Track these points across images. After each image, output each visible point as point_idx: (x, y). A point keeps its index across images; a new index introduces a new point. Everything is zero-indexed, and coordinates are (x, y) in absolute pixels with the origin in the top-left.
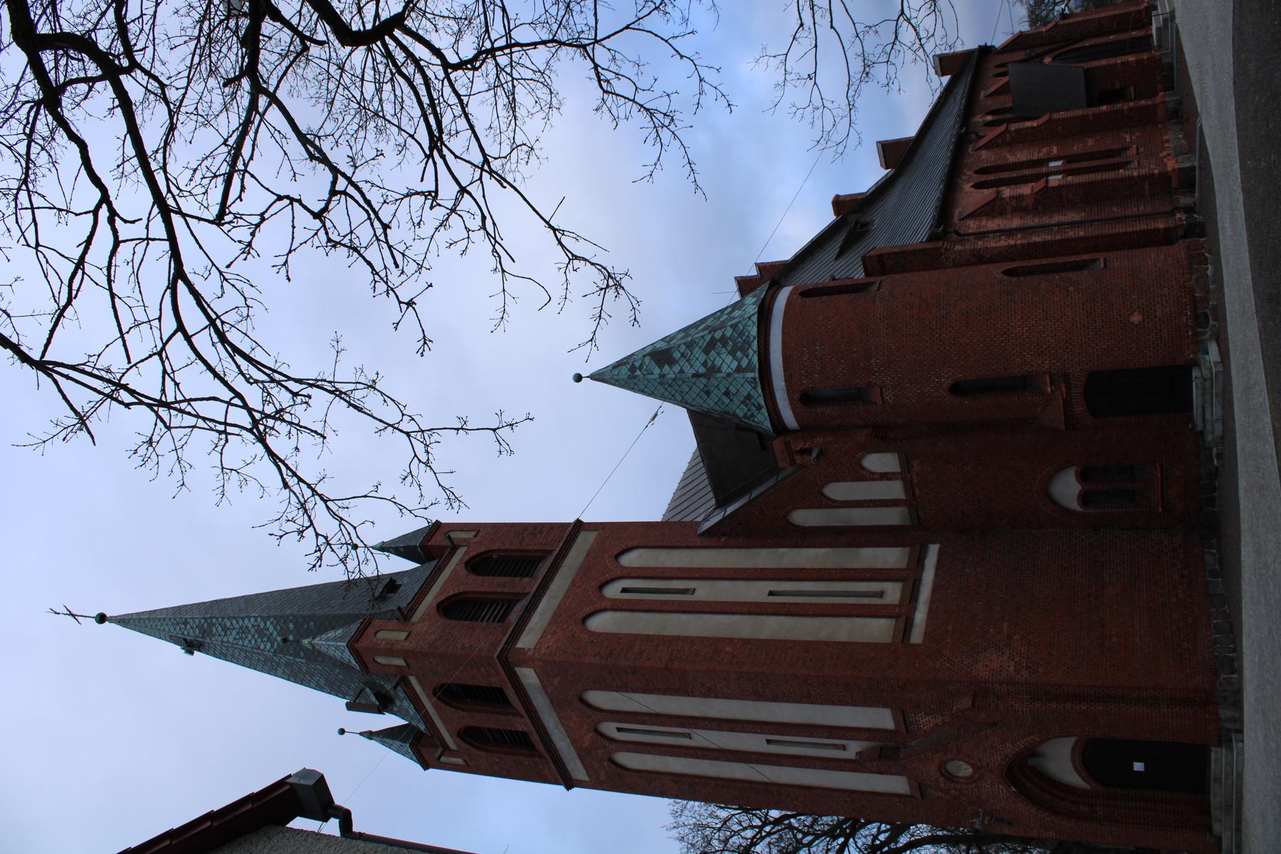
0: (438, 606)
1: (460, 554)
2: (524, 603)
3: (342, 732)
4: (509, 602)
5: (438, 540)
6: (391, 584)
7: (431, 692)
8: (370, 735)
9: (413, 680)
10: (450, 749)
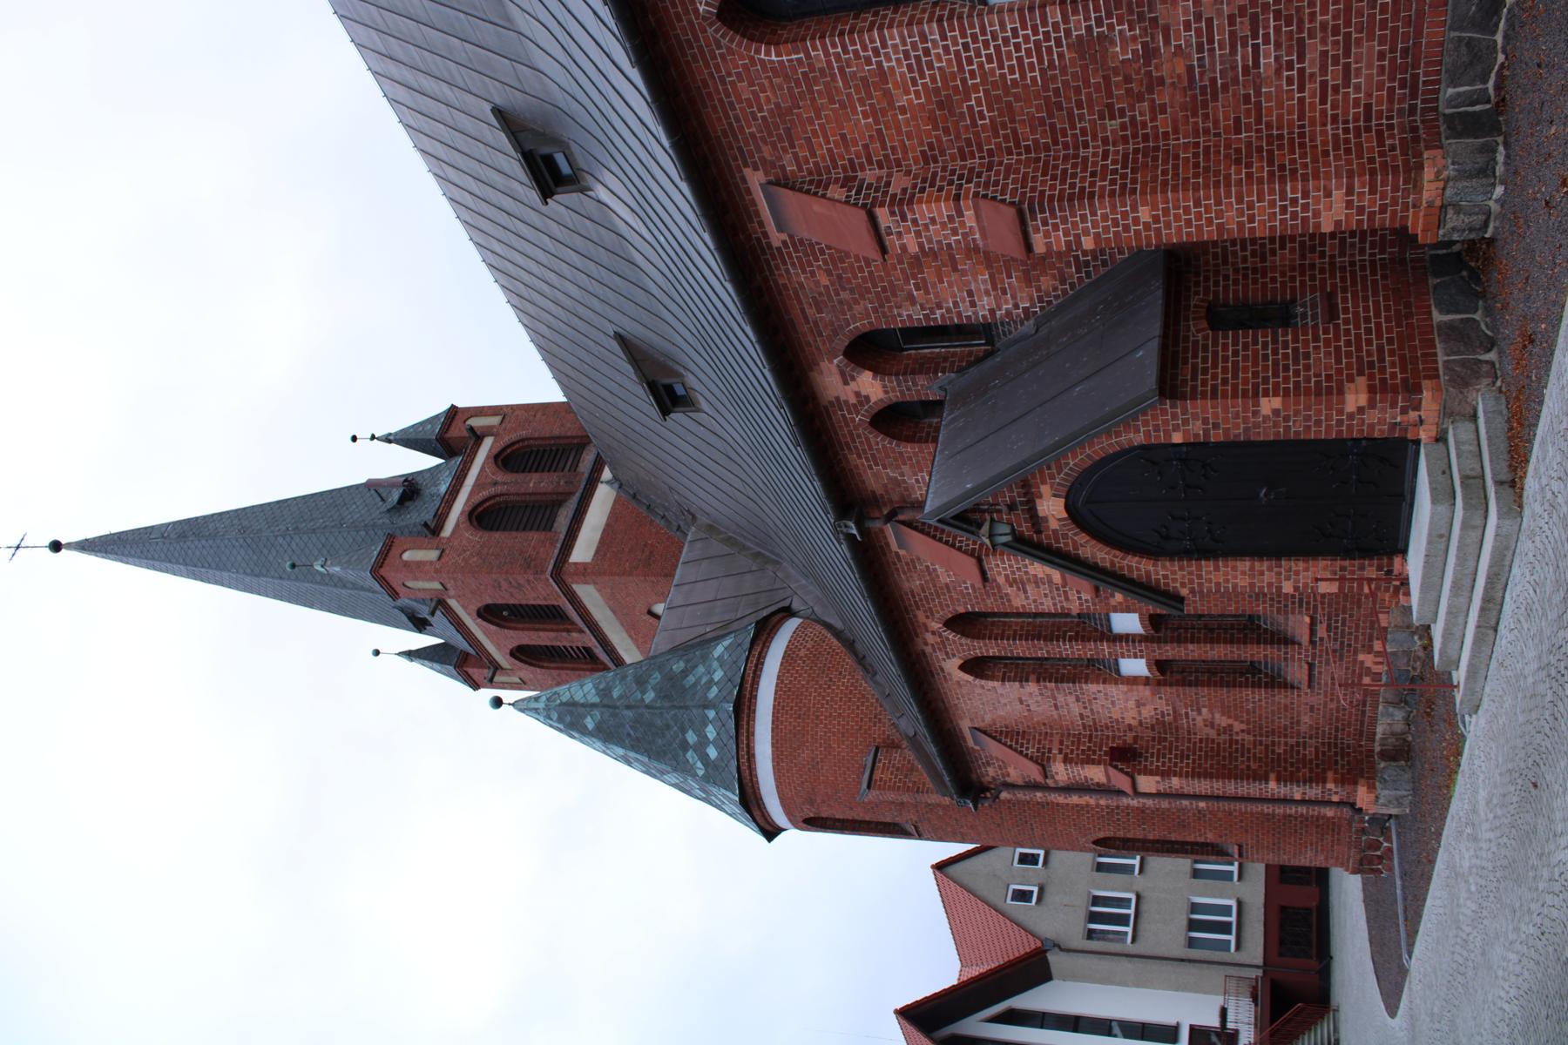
0: (471, 514)
1: (487, 446)
2: (572, 504)
3: (377, 653)
4: (552, 504)
5: (457, 431)
6: (410, 488)
7: (475, 614)
8: (410, 655)
9: (453, 603)
10: (502, 669)
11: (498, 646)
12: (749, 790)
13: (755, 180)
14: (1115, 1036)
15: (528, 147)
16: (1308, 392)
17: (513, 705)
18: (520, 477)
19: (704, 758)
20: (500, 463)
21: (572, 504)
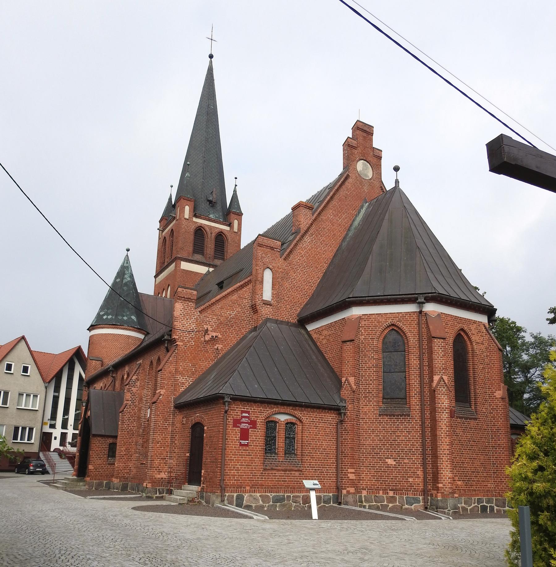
11: (166, 233)
12: (95, 327)
13: (141, 361)
14: (76, 411)
15: (224, 282)
16: (264, 461)
17: (127, 255)
18: (213, 242)
19: (103, 315)
20: (220, 233)
21: (204, 260)
